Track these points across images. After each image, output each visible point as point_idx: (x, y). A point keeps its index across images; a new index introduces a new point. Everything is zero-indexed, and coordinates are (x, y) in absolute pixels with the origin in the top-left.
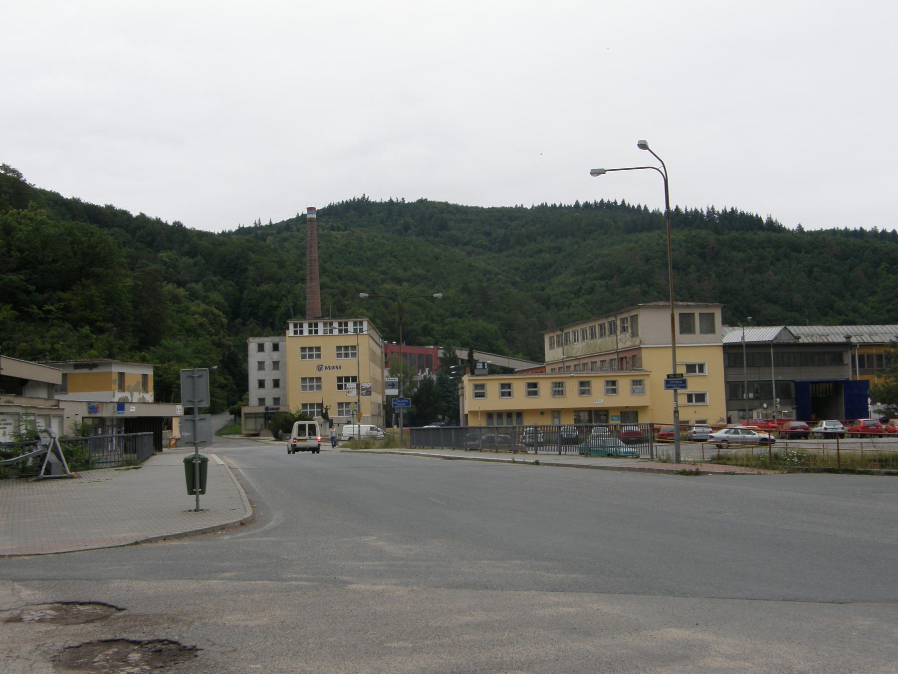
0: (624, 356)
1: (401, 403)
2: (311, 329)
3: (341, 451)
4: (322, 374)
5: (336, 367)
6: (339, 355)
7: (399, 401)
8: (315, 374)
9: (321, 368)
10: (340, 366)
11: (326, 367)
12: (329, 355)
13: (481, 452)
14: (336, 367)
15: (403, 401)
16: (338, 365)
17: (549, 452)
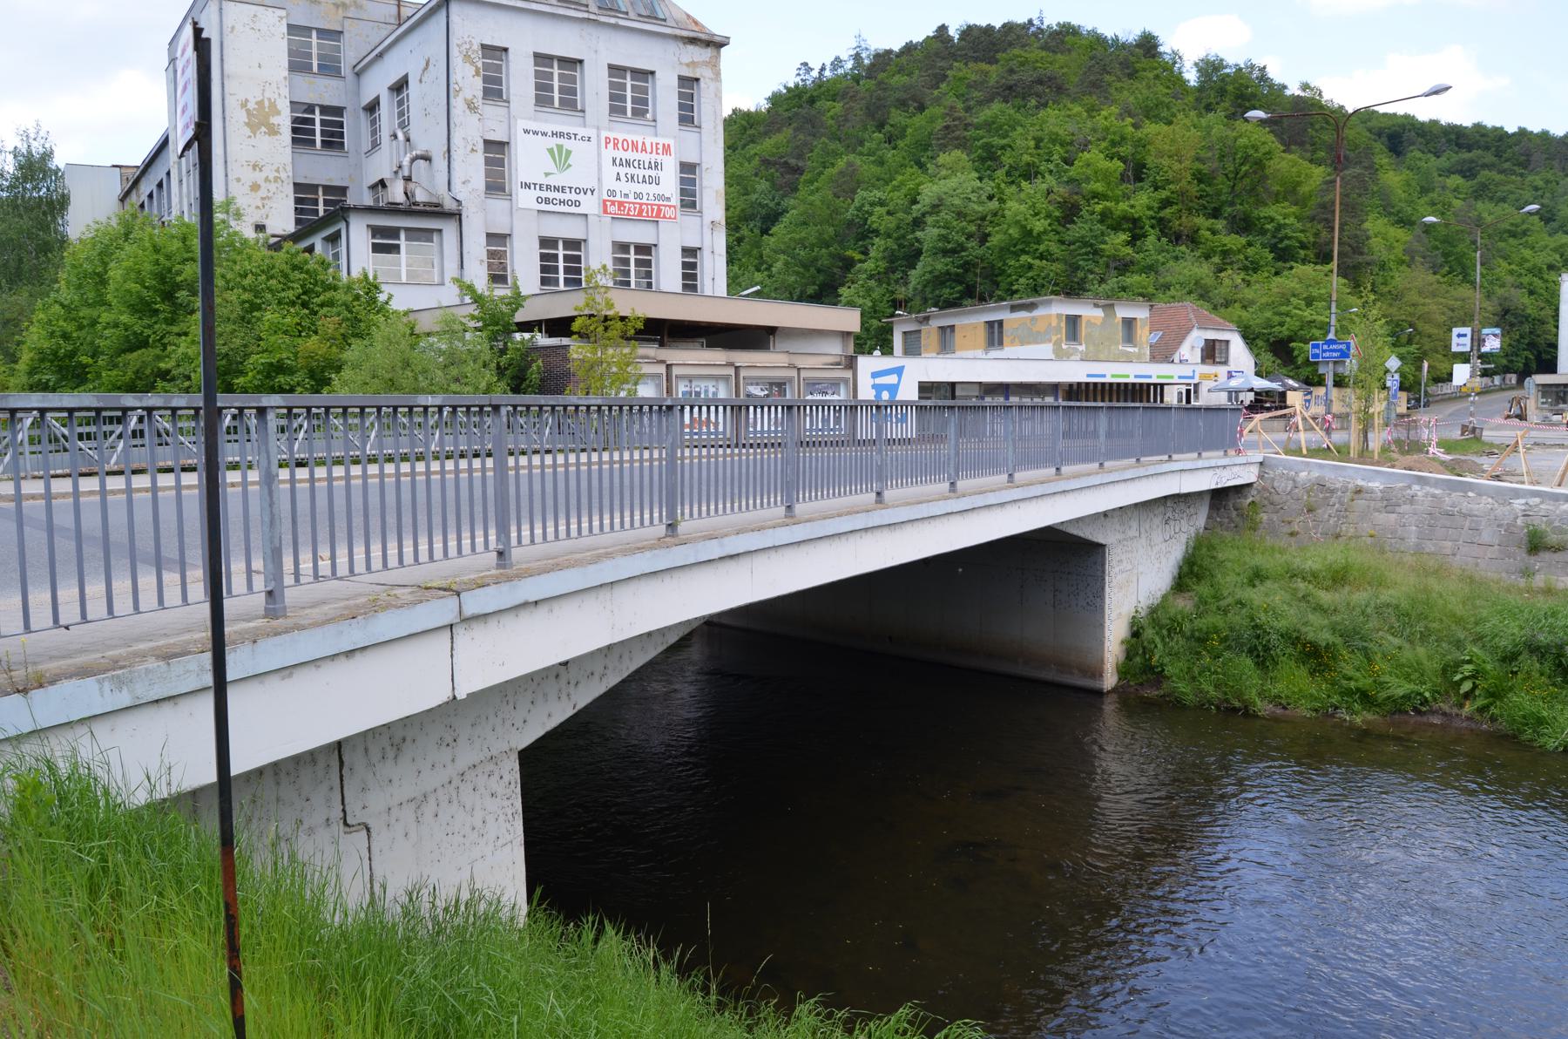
7: (1325, 347)
15: (1335, 347)
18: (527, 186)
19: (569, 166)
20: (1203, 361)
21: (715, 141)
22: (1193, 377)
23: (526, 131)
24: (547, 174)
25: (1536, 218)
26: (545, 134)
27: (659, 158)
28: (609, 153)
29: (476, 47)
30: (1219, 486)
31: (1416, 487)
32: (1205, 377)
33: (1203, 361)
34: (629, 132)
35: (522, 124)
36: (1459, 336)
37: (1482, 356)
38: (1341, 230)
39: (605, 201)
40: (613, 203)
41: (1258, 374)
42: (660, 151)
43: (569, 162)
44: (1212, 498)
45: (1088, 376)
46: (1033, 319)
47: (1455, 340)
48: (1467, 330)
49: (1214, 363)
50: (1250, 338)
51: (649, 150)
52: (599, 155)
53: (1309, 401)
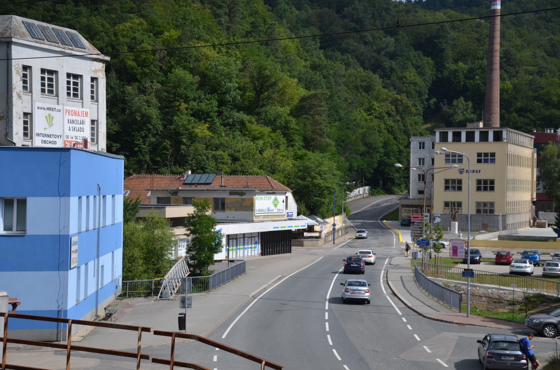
0: (193, 197)
2: (26, 120)
4: (464, 177)
5: (476, 171)
6: (479, 161)
9: (462, 172)
10: (480, 171)
13: (244, 234)
14: (476, 171)
16: (478, 169)
17: (502, 287)
18: (38, 135)
19: (53, 124)
21: (103, 109)
23: (38, 108)
24: (45, 129)
26: (44, 109)
27: (84, 118)
28: (67, 117)
29: (21, 67)
31: (464, 286)
34: (73, 106)
35: (37, 104)
39: (65, 141)
40: (68, 141)
42: (84, 115)
43: (53, 122)
45: (274, 228)
46: (243, 199)
51: (80, 115)
52: (63, 118)
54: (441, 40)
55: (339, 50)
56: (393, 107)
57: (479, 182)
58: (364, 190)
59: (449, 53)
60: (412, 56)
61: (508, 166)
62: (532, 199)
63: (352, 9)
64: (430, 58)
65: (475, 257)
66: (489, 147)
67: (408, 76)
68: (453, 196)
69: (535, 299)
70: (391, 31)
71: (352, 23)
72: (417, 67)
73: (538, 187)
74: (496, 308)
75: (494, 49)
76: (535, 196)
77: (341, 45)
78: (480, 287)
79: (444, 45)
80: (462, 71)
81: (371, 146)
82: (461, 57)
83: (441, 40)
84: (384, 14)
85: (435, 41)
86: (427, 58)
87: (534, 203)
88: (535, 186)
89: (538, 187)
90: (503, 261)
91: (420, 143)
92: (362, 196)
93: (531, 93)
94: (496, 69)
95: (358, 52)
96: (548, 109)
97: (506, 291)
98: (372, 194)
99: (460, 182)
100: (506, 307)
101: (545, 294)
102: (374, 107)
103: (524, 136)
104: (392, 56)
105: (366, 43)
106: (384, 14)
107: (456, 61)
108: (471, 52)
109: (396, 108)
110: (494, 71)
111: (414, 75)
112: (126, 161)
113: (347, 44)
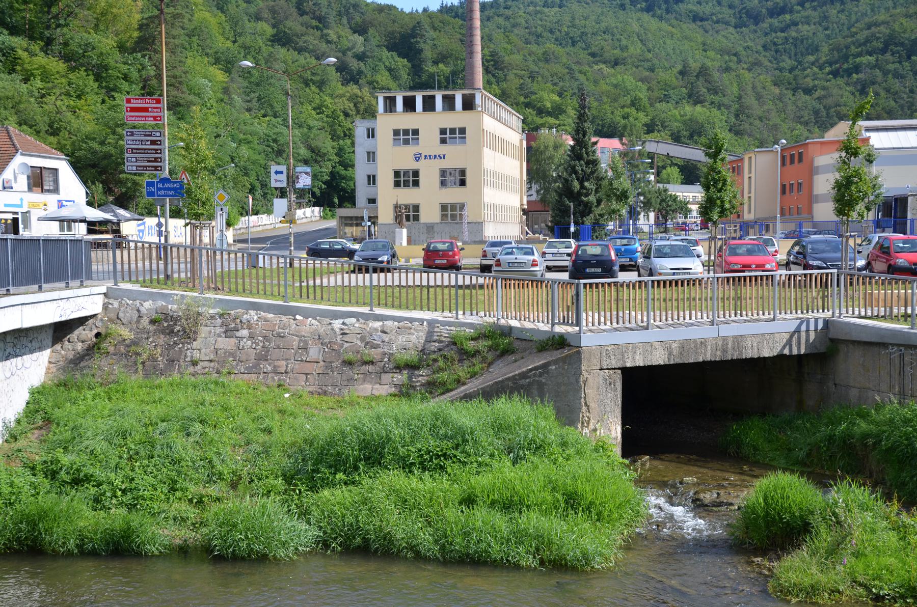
1: (165, 189)
3: (691, 269)
4: (421, 166)
6: (443, 141)
7: (160, 185)
8: (412, 165)
9: (419, 158)
10: (444, 155)
11: (426, 156)
12: (429, 141)
15: (169, 185)
16: (442, 154)
17: (378, 311)
20: (30, 189)
22: (21, 206)
25: (333, 69)
30: (64, 319)
31: (252, 312)
32: (35, 205)
33: (30, 189)
36: (277, 173)
37: (296, 191)
38: (162, 42)
41: (90, 204)
44: (55, 332)
47: (273, 176)
48: (283, 168)
49: (43, 191)
50: (78, 167)
53: (142, 231)
54: (418, 39)
55: (295, 49)
56: (352, 105)
57: (443, 173)
58: (313, 212)
59: (428, 53)
60: (384, 57)
61: (485, 148)
62: (522, 205)
63: (313, 4)
64: (406, 60)
65: (380, 256)
66: (457, 118)
67: (380, 80)
68: (407, 196)
69: (482, 345)
70: (360, 30)
71: (314, 21)
72: (390, 70)
73: (530, 193)
74: (351, 380)
75: (474, 26)
76: (525, 202)
77: (298, 44)
78: (307, 313)
79: (422, 45)
80: (444, 75)
81: (319, 151)
82: (442, 58)
83: (418, 39)
84: (351, 10)
85: (412, 40)
86: (402, 60)
87: (525, 212)
88: (525, 186)
89: (530, 193)
90: (439, 262)
91: (368, 130)
92: (309, 220)
93: (522, 99)
94: (477, 52)
95: (318, 52)
96: (542, 118)
97: (389, 323)
98: (324, 218)
99: (416, 173)
100: (386, 378)
101: (514, 323)
102: (326, 103)
103: (508, 111)
104: (361, 57)
105: (328, 42)
106: (351, 10)
107: (436, 63)
108: (454, 52)
109: (355, 105)
110: (475, 54)
111: (386, 79)
112: (544, 338)
113: (305, 42)
